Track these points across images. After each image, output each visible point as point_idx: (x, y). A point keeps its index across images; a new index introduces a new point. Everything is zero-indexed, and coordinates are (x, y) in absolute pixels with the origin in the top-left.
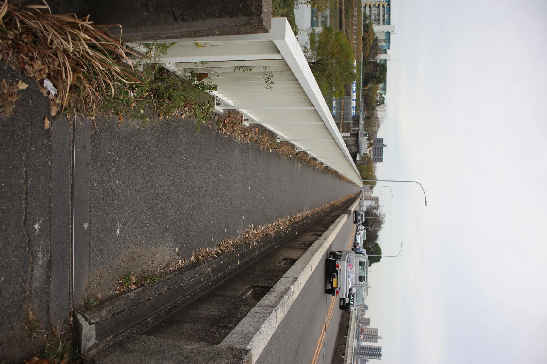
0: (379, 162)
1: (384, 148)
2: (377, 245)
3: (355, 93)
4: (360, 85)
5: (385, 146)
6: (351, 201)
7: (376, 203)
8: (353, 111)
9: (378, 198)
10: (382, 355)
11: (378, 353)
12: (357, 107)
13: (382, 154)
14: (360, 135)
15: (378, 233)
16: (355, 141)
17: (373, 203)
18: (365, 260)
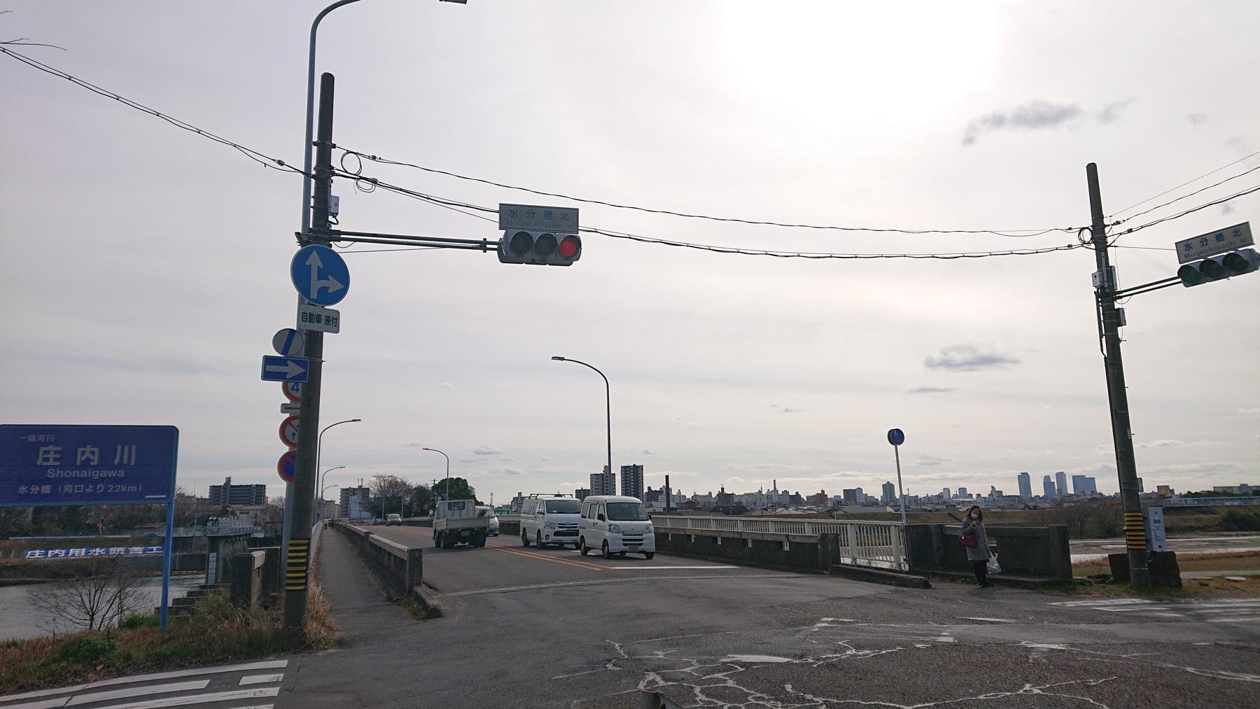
0: (265, 492)
1: (233, 483)
2: (435, 487)
3: (111, 549)
4: (92, 539)
5: (228, 480)
6: (352, 536)
7: (354, 494)
8: (152, 550)
9: (622, 467)
10: (634, 465)
11: (632, 471)
12: (146, 542)
13: (248, 486)
14: (214, 533)
15: (284, 496)
16: (227, 542)
17: (355, 499)
18: (32, 509)
